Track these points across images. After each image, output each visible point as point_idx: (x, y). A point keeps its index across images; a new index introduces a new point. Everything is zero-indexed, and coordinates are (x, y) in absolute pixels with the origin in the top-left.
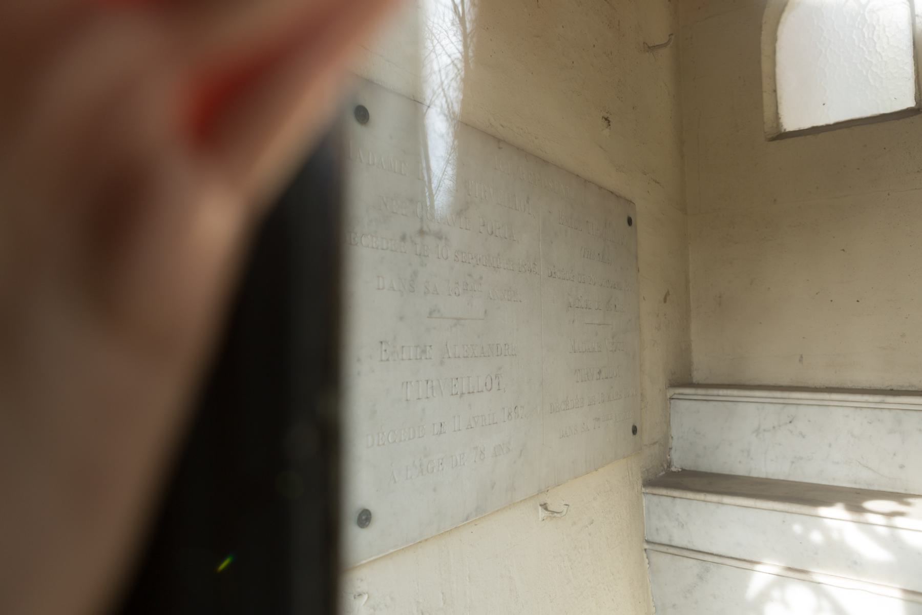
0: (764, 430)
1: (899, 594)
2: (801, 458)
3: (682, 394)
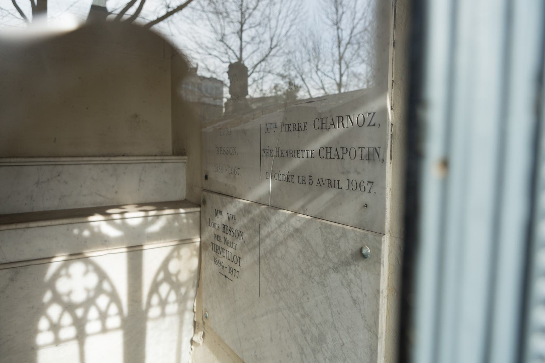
0: (42, 182)
1: (125, 250)
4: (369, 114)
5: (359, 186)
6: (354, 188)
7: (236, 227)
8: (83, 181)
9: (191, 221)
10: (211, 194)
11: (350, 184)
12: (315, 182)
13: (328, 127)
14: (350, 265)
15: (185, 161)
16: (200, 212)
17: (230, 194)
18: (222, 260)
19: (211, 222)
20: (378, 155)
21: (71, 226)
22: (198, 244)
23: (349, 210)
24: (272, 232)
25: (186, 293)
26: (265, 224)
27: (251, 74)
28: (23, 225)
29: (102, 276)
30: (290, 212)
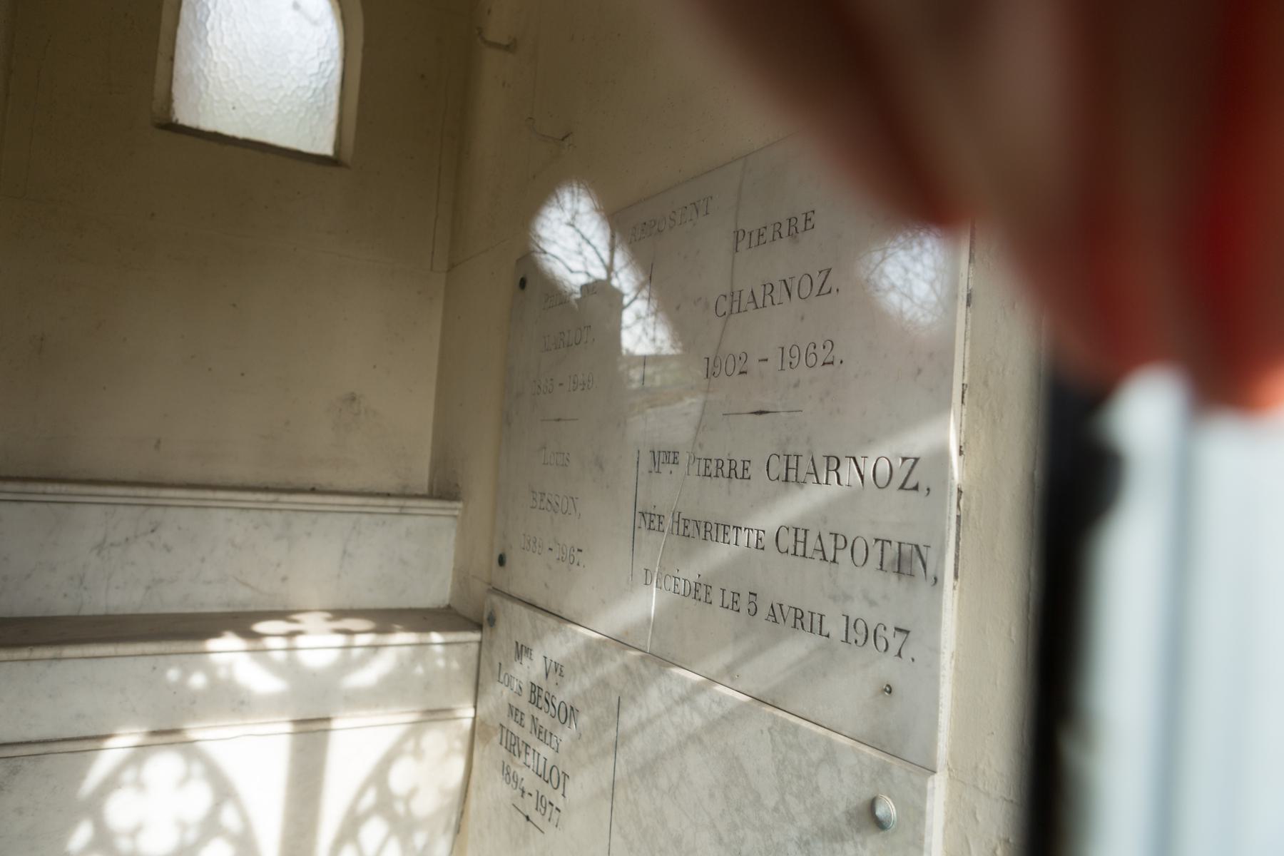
0: (112, 545)
1: (288, 728)
2: (161, 581)
3: (157, 498)
4: (904, 459)
5: (872, 635)
6: (861, 641)
7: (566, 693)
8: (209, 549)
9: (455, 665)
10: (509, 604)
11: (851, 629)
12: (764, 610)
13: (801, 478)
14: (843, 840)
15: (457, 513)
16: (480, 643)
17: (553, 608)
18: (522, 773)
19: (503, 673)
20: (924, 565)
21: (161, 659)
22: (467, 723)
23: (847, 691)
24: (650, 721)
25: (427, 847)
26: (633, 699)
27: (631, 302)
28: (48, 652)
29: (223, 791)
30: (697, 678)
